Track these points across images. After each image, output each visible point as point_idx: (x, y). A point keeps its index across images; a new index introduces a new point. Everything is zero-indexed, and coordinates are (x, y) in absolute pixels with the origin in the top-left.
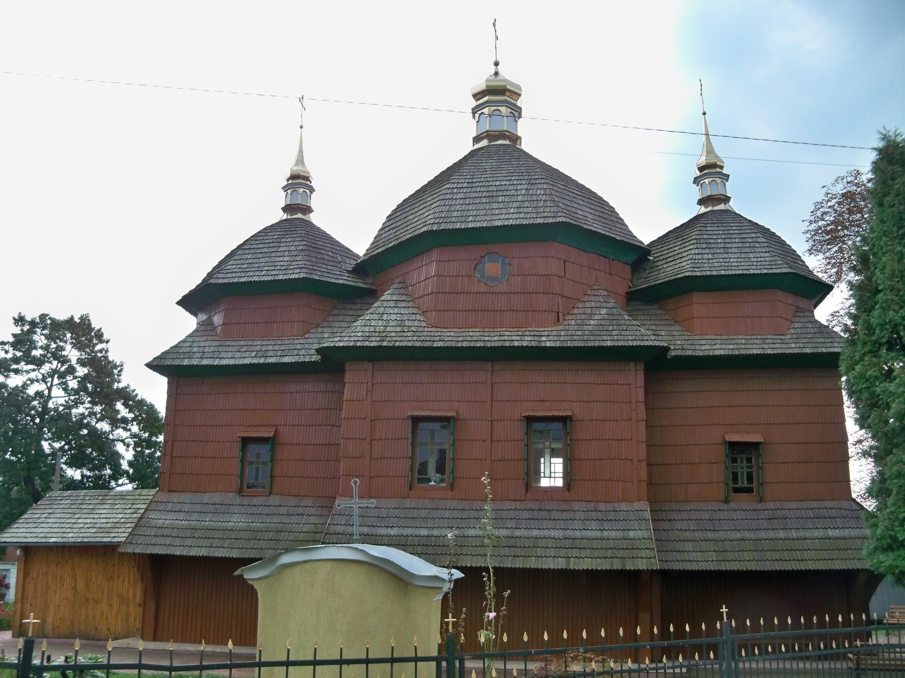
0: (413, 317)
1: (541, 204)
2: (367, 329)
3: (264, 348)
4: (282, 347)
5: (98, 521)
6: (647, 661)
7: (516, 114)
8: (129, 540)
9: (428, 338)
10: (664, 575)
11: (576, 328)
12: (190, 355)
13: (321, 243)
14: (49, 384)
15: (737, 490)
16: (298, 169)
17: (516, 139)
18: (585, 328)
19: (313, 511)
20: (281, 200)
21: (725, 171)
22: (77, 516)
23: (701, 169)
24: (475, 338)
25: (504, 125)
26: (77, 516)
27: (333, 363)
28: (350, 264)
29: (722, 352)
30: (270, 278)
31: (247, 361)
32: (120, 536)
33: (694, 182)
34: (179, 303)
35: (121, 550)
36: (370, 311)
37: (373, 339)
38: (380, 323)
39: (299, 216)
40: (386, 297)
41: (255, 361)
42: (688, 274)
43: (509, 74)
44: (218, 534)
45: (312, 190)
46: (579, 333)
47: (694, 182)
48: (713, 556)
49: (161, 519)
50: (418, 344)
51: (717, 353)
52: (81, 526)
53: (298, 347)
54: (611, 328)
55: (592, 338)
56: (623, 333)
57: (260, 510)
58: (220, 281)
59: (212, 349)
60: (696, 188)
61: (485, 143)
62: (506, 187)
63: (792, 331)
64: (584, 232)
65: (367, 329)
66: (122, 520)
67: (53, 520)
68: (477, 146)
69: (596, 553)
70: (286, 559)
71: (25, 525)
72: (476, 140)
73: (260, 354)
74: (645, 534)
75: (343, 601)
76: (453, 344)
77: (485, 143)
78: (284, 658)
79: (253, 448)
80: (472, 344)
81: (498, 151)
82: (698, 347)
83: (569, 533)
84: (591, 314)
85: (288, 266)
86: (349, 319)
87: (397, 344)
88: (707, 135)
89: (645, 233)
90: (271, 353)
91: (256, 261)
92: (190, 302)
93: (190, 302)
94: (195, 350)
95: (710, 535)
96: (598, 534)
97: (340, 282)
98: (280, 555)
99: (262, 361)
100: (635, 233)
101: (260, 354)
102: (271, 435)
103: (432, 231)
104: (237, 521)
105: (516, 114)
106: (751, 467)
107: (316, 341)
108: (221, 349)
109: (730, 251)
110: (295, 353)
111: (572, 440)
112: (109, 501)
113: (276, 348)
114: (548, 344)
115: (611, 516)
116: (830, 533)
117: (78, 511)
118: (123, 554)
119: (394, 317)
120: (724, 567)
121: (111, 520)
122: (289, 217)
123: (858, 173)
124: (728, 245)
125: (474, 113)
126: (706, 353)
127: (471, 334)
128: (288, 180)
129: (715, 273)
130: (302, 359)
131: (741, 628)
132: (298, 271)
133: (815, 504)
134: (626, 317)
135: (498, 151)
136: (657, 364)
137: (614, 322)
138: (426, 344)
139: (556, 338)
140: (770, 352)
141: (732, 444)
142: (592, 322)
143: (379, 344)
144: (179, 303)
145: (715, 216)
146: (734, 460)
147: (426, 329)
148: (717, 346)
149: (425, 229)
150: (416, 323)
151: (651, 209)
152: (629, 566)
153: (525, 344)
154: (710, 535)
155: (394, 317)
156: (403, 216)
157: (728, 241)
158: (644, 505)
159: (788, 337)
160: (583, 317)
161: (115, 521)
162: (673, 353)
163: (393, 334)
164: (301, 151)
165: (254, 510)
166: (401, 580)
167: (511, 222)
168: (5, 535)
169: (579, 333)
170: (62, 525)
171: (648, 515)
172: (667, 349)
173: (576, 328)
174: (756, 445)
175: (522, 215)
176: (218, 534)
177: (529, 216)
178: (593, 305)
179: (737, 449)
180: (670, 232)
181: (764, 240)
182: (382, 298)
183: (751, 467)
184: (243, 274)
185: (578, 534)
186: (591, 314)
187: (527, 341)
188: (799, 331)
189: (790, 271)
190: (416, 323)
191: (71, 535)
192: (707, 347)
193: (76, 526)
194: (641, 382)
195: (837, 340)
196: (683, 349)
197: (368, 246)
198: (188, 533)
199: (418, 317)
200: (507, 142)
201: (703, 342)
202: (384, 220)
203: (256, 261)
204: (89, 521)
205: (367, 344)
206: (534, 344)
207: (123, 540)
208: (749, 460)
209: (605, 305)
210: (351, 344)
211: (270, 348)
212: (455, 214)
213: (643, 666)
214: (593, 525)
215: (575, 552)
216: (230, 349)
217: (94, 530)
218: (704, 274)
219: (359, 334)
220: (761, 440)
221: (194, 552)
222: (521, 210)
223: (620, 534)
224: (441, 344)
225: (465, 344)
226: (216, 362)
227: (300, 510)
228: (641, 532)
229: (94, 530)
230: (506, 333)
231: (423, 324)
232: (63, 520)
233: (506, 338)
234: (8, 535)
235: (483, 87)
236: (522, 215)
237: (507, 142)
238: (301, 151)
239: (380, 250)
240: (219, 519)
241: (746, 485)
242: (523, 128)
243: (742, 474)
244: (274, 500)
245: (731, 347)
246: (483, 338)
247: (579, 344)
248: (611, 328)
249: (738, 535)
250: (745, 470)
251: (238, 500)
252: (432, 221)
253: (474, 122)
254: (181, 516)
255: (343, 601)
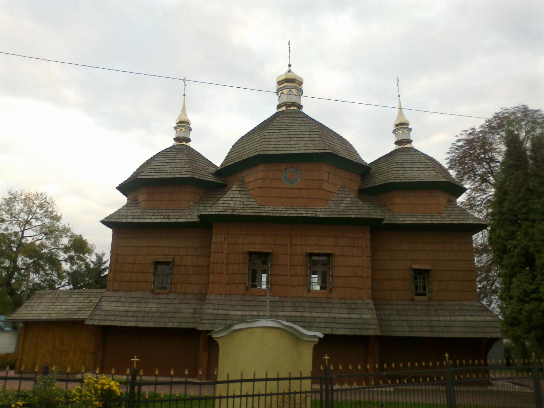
0: (249, 200)
1: (317, 142)
2: (225, 205)
3: (168, 214)
4: (178, 214)
5: (69, 307)
6: (364, 384)
7: (300, 93)
8: (90, 318)
9: (258, 211)
10: (380, 339)
11: (334, 207)
12: (126, 217)
13: (195, 157)
14: (22, 229)
15: (417, 295)
16: (182, 119)
17: (300, 107)
18: (340, 208)
19: (193, 301)
20: (173, 134)
21: (409, 127)
22: (57, 304)
23: (397, 125)
24: (282, 212)
25: (294, 99)
26: (57, 304)
27: (206, 223)
28: (213, 170)
29: (410, 222)
30: (171, 177)
31: (159, 221)
32: (83, 315)
33: (393, 132)
34: (118, 188)
35: (87, 323)
36: (226, 196)
37: (229, 211)
38: (232, 202)
39: (184, 143)
40: (234, 188)
41: (163, 221)
42: (392, 181)
43: (298, 72)
44: (141, 314)
45: (190, 129)
46: (336, 210)
47: (393, 132)
48: (407, 329)
49: (107, 306)
50: (253, 214)
51: (408, 222)
52: (59, 309)
53: (186, 214)
54: (352, 208)
55: (343, 213)
56: (360, 211)
57: (163, 301)
58: (144, 177)
59: (138, 214)
60: (394, 135)
61: (284, 108)
62: (298, 133)
63: (446, 212)
64: (334, 157)
65: (225, 205)
66: (83, 307)
67: (42, 307)
68: (279, 110)
69: (346, 326)
70: (237, 327)
71: (25, 309)
72: (279, 107)
73: (166, 217)
74: (372, 317)
75: (262, 349)
76: (272, 215)
77: (284, 108)
78: (299, 376)
79: (160, 267)
80: (281, 215)
81: (290, 113)
82: (397, 219)
83: (332, 315)
84: (342, 201)
85: (179, 170)
86: (214, 199)
87: (242, 214)
88: (400, 108)
89: (368, 158)
90: (172, 217)
91: (163, 167)
92: (123, 188)
93: (123, 188)
94: (129, 214)
95: (404, 318)
96: (347, 316)
97: (209, 180)
98: (234, 324)
99: (167, 221)
100: (363, 159)
101: (166, 217)
102: (171, 260)
103: (260, 155)
104: (152, 306)
105: (300, 93)
106: (425, 283)
107: (196, 211)
108: (144, 214)
109: (414, 169)
110: (185, 217)
111: (332, 266)
112: (74, 296)
113: (174, 214)
114: (321, 216)
115: (353, 306)
116: (468, 318)
117: (56, 301)
118: (87, 325)
119: (239, 199)
120: (412, 335)
121: (76, 307)
122: (178, 144)
123: (475, 129)
124: (413, 166)
125: (277, 93)
126: (402, 222)
127: (280, 209)
128: (177, 124)
129: (407, 181)
130: (189, 220)
131: (455, 365)
132: (186, 173)
133: (458, 303)
134: (360, 203)
135: (290, 113)
136: (376, 228)
137: (354, 205)
138: (257, 214)
139: (325, 213)
140: (436, 222)
141: (416, 271)
142: (343, 205)
143: (232, 213)
144: (118, 188)
145: (404, 150)
146: (416, 279)
147: (256, 206)
148: (408, 219)
149: (256, 154)
150: (251, 203)
151: (371, 146)
152: (364, 333)
153: (309, 215)
154: (404, 318)
155: (239, 199)
156: (243, 146)
157: (412, 164)
158: (370, 301)
159: (445, 215)
160: (338, 202)
161: (79, 307)
162: (384, 222)
163: (239, 208)
164: (184, 108)
165: (160, 301)
166: (297, 338)
167: (301, 152)
168: (14, 315)
169: (336, 210)
170: (48, 309)
171: (372, 306)
172: (382, 220)
173: (334, 207)
174: (428, 271)
175: (307, 148)
176: (141, 314)
177: (311, 148)
178: (343, 195)
179: (418, 272)
180: (380, 158)
181: (431, 164)
182: (232, 189)
183: (425, 283)
184: (156, 174)
185: (336, 315)
186: (342, 201)
187: (310, 214)
188: (450, 212)
189: (446, 180)
190: (251, 203)
191: (54, 315)
192: (402, 219)
193: (56, 310)
194: (369, 237)
195: (471, 217)
196: (390, 220)
197: (222, 161)
198: (124, 314)
199: (252, 200)
200: (296, 108)
201: (400, 216)
202: (231, 147)
203: (163, 167)
204: (64, 307)
205: (225, 213)
206: (314, 216)
207: (87, 317)
208: (424, 279)
209: (349, 196)
210: (217, 213)
211: (171, 214)
212: (272, 146)
213: (362, 386)
214: (345, 311)
215: (335, 325)
216: (149, 214)
217: (67, 312)
218: (401, 181)
219: (221, 208)
220: (430, 268)
221: (128, 324)
222: (306, 145)
223: (359, 316)
224: (265, 214)
225: (278, 215)
226: (142, 221)
227: (186, 301)
228: (369, 315)
229: (67, 312)
230: (299, 210)
231: (255, 203)
232: (48, 307)
233: (299, 212)
234: (17, 315)
235: (283, 78)
236: (307, 148)
237: (296, 108)
238: (184, 108)
239: (230, 164)
240: (169, 309)
241: (422, 292)
242: (303, 101)
243: (420, 286)
244: (172, 296)
245: (415, 219)
246: (287, 212)
247: (337, 216)
248: (352, 208)
249: (419, 318)
250: (422, 284)
251: (151, 296)
252: (260, 150)
253: (277, 97)
254: (120, 304)
255: (262, 349)
